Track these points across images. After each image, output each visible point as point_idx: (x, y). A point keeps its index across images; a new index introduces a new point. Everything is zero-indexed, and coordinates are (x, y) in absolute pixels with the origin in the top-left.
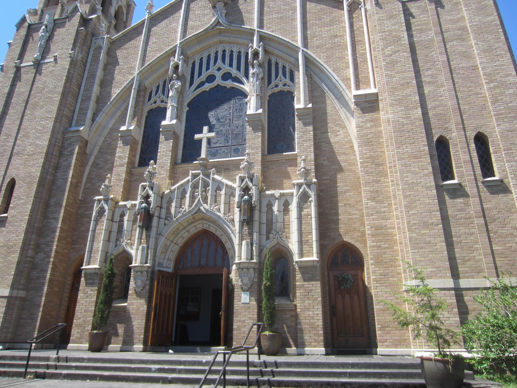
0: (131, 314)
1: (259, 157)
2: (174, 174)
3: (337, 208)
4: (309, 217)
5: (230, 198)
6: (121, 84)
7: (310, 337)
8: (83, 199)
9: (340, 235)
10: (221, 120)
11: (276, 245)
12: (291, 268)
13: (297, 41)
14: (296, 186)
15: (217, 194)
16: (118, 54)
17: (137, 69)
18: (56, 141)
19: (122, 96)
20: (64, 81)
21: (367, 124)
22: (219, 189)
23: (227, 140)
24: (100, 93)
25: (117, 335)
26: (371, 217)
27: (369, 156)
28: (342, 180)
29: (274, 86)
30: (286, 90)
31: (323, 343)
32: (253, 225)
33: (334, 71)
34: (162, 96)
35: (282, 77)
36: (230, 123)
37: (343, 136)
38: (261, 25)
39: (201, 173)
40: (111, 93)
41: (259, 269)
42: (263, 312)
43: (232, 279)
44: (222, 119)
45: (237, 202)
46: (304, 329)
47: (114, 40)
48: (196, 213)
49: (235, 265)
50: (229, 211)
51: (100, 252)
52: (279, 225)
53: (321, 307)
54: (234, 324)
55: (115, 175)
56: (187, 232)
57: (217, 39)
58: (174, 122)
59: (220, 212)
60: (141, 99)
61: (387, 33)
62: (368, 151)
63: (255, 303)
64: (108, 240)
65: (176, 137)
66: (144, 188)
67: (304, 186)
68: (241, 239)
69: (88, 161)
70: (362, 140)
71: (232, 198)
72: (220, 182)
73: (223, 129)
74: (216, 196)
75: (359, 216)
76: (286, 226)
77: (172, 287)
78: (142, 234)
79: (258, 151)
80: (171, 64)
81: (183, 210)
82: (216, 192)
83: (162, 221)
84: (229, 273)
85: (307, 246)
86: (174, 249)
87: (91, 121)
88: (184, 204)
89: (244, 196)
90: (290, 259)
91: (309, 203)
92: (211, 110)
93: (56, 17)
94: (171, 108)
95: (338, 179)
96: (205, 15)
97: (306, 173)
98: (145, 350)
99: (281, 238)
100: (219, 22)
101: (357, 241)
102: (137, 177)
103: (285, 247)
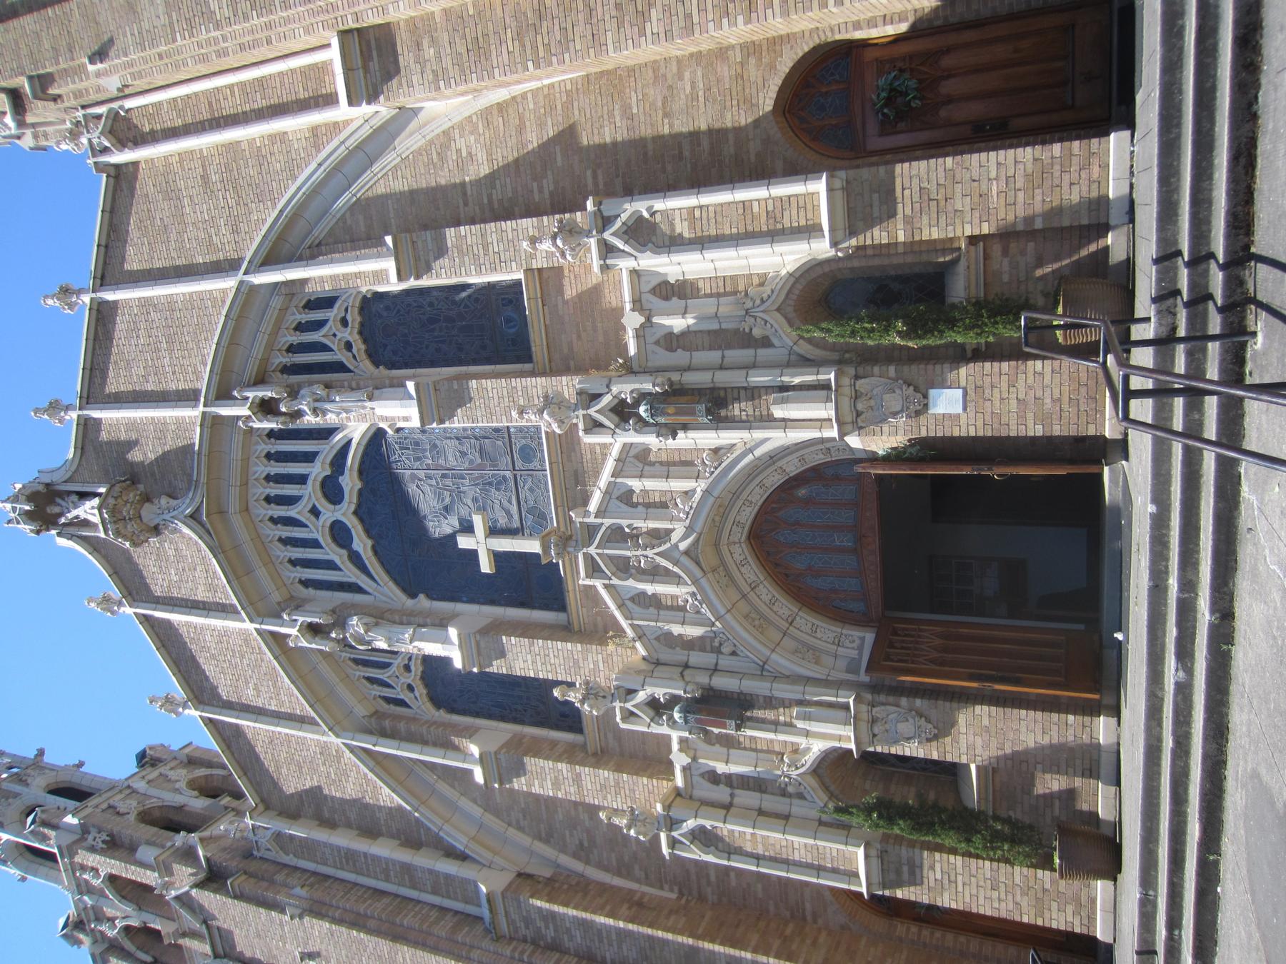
0: (1000, 753)
1: (538, 386)
2: (596, 632)
3: (676, 138)
4: (697, 213)
5: (652, 464)
6: (368, 781)
7: (1071, 184)
8: (676, 889)
9: (757, 123)
10: (447, 500)
11: (786, 318)
12: (856, 263)
13: (224, 291)
14: (608, 262)
15: (641, 501)
16: (292, 790)
17: (325, 739)
18: (519, 960)
19: (397, 780)
20: (362, 935)
21: (427, 57)
22: (627, 497)
23: (499, 483)
24: (392, 836)
25: (1070, 795)
26: (696, 20)
27: (516, 43)
28: (596, 131)
29: (350, 354)
30: (358, 319)
31: (1095, 141)
32: (725, 389)
33: (295, 178)
34: (393, 669)
35: (324, 330)
36: (454, 477)
37: (472, 138)
38: (188, 397)
39: (585, 550)
40: (390, 808)
41: (846, 358)
42: (991, 339)
43: (892, 448)
44: (443, 500)
45: (658, 436)
46: (1047, 207)
47: (258, 800)
48: (698, 563)
49: (847, 439)
50: (690, 464)
51: (819, 843)
52: (726, 307)
53: (975, 156)
54: (1031, 434)
55: (605, 798)
56: (757, 590)
57: (237, 521)
58: (453, 632)
59: (694, 491)
60: (402, 726)
61: (174, 18)
62: (504, 46)
63: (963, 371)
64: (784, 820)
65: (496, 628)
66: (629, 715)
67: (607, 235)
68: (768, 421)
69: (571, 873)
70: (473, 69)
71: (652, 458)
72: (607, 493)
73: (471, 494)
74: (648, 506)
75: (700, 69)
76: (727, 289)
77: (921, 630)
78: (763, 721)
79: (519, 388)
80: (305, 644)
81: (690, 600)
82: (635, 505)
83: (725, 662)
84: (873, 459)
85: (786, 214)
86: (807, 628)
87: (465, 864)
88: (673, 597)
89: (640, 419)
90: (827, 269)
91: (658, 217)
92: (423, 530)
93: (207, 949)
94: (416, 644)
95: (591, 143)
96: (179, 555)
97: (570, 232)
98: (1116, 712)
99: (763, 301)
100: (192, 516)
101: (772, 67)
102: (610, 736)
103: (793, 286)
